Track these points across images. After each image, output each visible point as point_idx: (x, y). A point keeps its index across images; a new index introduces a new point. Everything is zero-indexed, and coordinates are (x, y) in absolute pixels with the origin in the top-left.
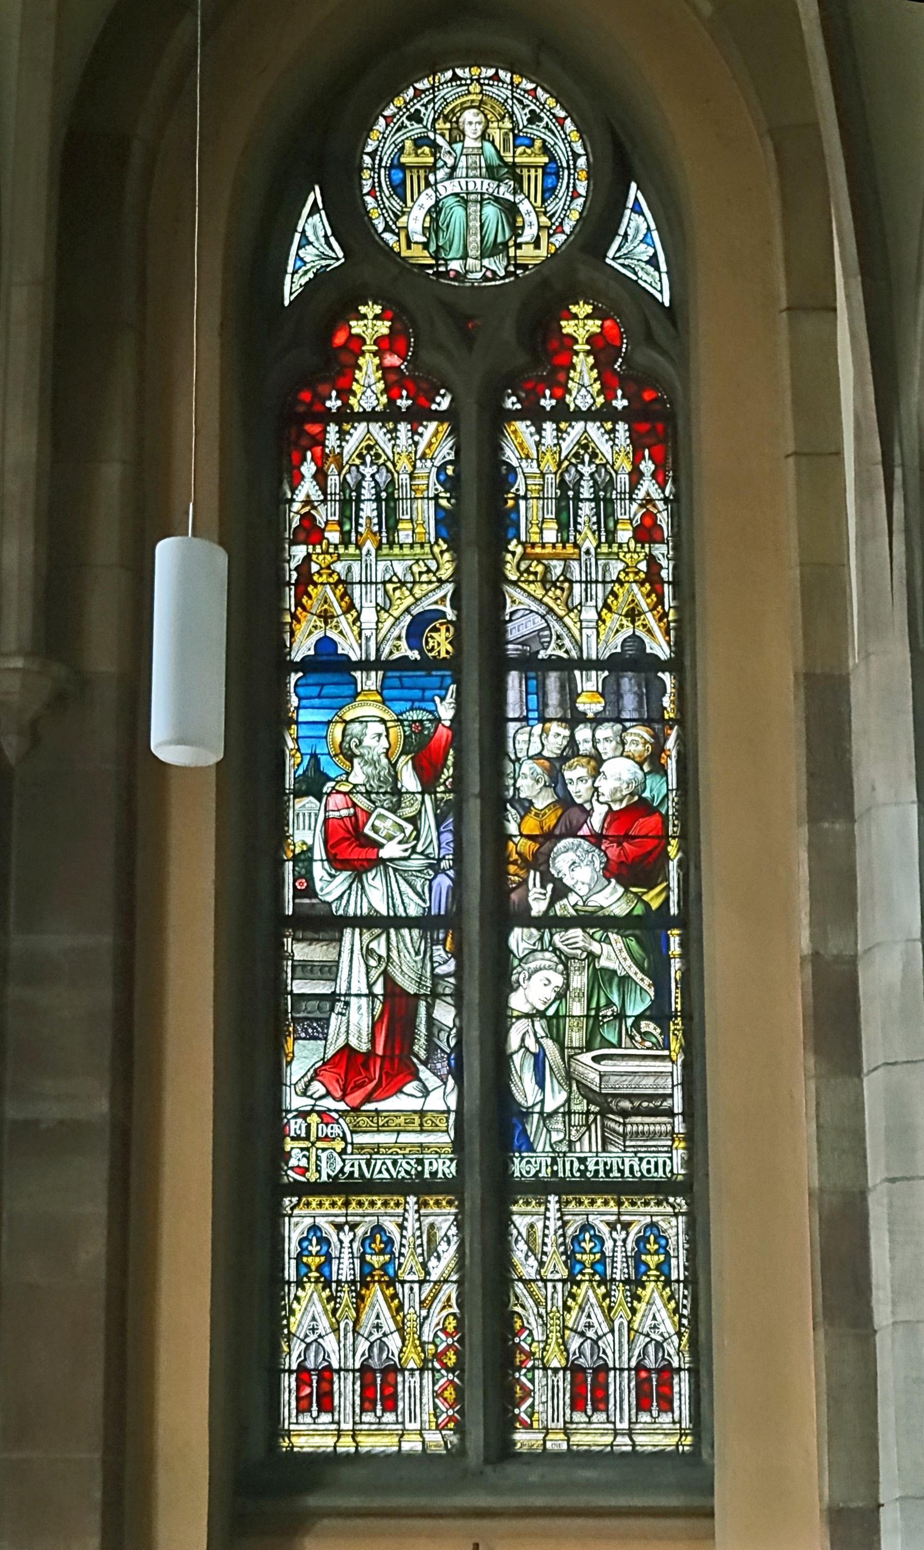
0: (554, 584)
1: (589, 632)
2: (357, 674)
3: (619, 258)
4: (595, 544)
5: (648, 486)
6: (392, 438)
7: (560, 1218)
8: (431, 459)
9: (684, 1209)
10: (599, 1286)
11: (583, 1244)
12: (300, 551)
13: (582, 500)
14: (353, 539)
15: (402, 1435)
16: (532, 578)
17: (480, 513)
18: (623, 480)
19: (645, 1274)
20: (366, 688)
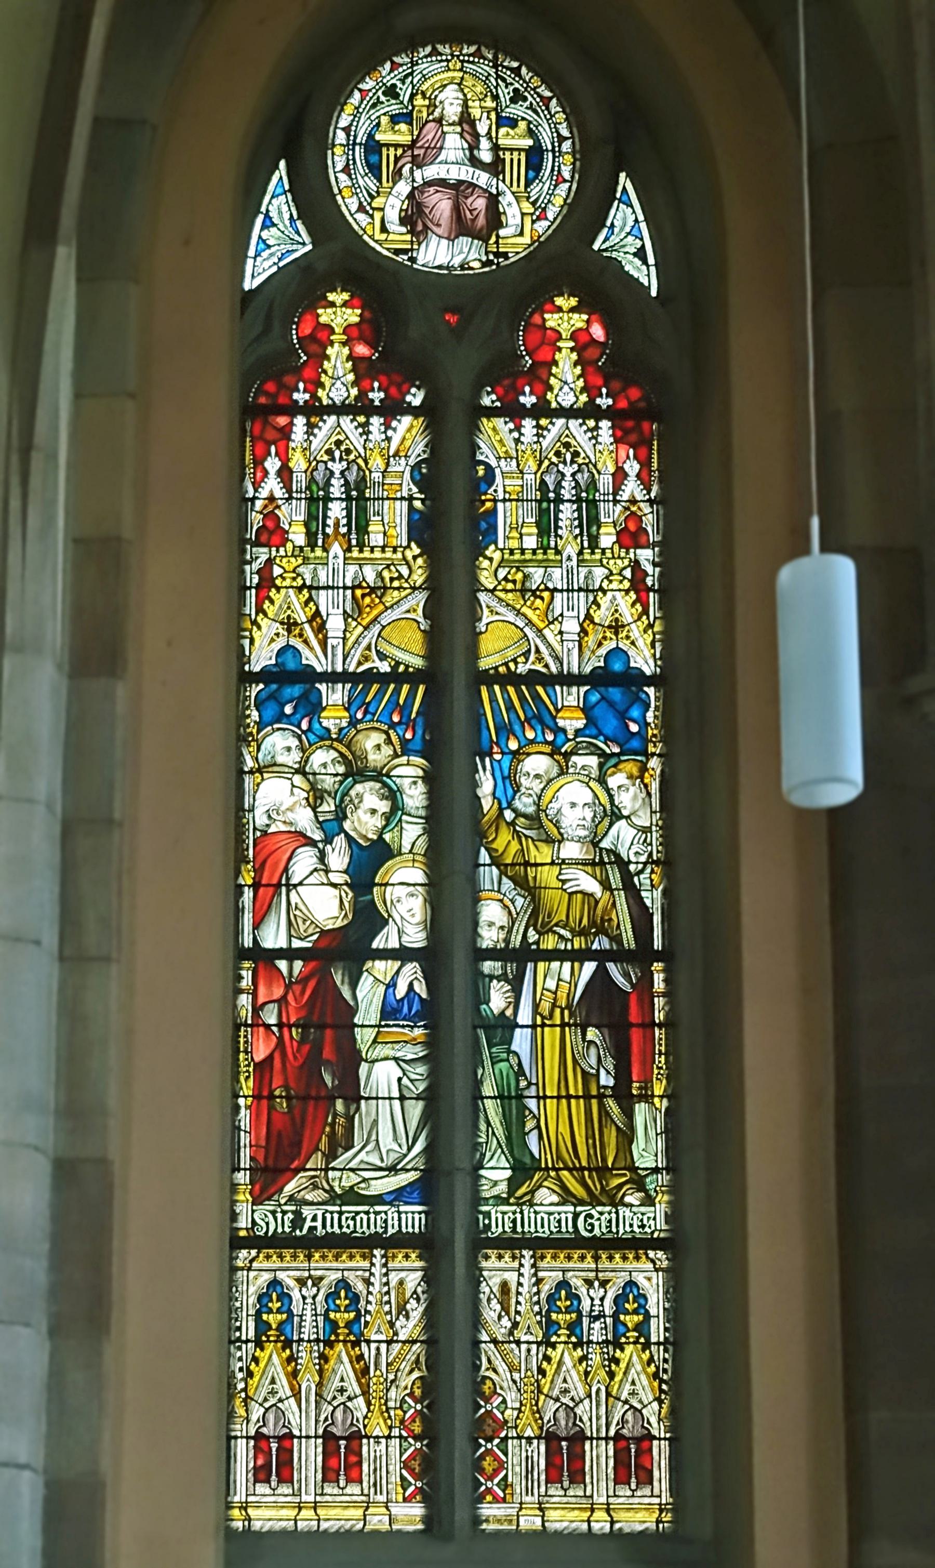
0: (534, 592)
1: (571, 645)
2: (322, 687)
3: (299, 243)
4: (577, 549)
5: (632, 488)
6: (593, 437)
7: (535, 1275)
8: (406, 456)
9: (665, 1264)
10: (575, 1349)
11: (559, 1303)
12: (263, 554)
13: (332, 500)
14: (320, 542)
15: (367, 1508)
16: (510, 586)
17: (451, 518)
18: (605, 482)
19: (624, 1335)
20: (566, 704)
